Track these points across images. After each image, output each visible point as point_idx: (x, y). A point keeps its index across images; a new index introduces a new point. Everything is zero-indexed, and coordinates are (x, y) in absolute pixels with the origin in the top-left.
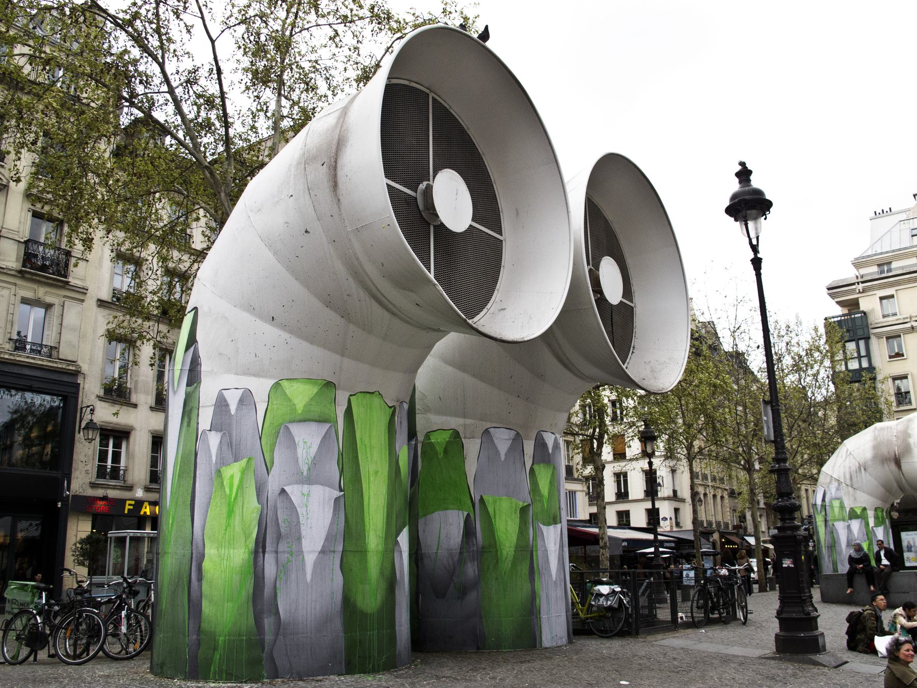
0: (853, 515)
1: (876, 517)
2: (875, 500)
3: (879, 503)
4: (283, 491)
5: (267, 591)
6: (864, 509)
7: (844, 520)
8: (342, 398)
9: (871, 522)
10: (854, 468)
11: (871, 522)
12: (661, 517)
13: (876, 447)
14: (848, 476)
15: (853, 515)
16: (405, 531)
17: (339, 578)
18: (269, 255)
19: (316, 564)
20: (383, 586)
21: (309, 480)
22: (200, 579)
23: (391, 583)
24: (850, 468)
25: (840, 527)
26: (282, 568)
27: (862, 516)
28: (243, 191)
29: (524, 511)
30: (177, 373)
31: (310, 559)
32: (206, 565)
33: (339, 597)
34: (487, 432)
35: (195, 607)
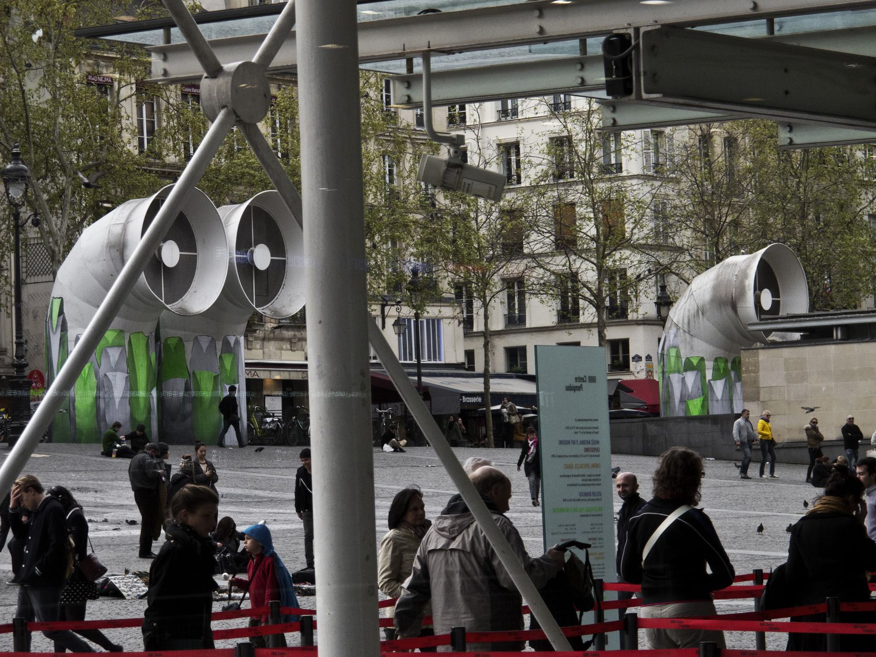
0: (689, 366)
1: (716, 369)
2: (715, 349)
3: (720, 353)
4: (105, 375)
5: (102, 413)
6: (702, 359)
7: (679, 372)
8: (127, 335)
9: (709, 375)
10: (692, 312)
11: (709, 375)
12: (632, 354)
13: (716, 288)
14: (686, 321)
15: (689, 366)
16: (155, 389)
17: (128, 408)
18: (96, 282)
19: (120, 402)
20: (146, 411)
21: (116, 369)
22: (74, 409)
23: (149, 411)
24: (689, 311)
25: (675, 378)
26: (107, 405)
27: (699, 368)
28: (73, 245)
29: (216, 378)
30: (54, 326)
31: (117, 401)
32: (77, 404)
33: (129, 415)
34: (196, 338)
35: (72, 420)
